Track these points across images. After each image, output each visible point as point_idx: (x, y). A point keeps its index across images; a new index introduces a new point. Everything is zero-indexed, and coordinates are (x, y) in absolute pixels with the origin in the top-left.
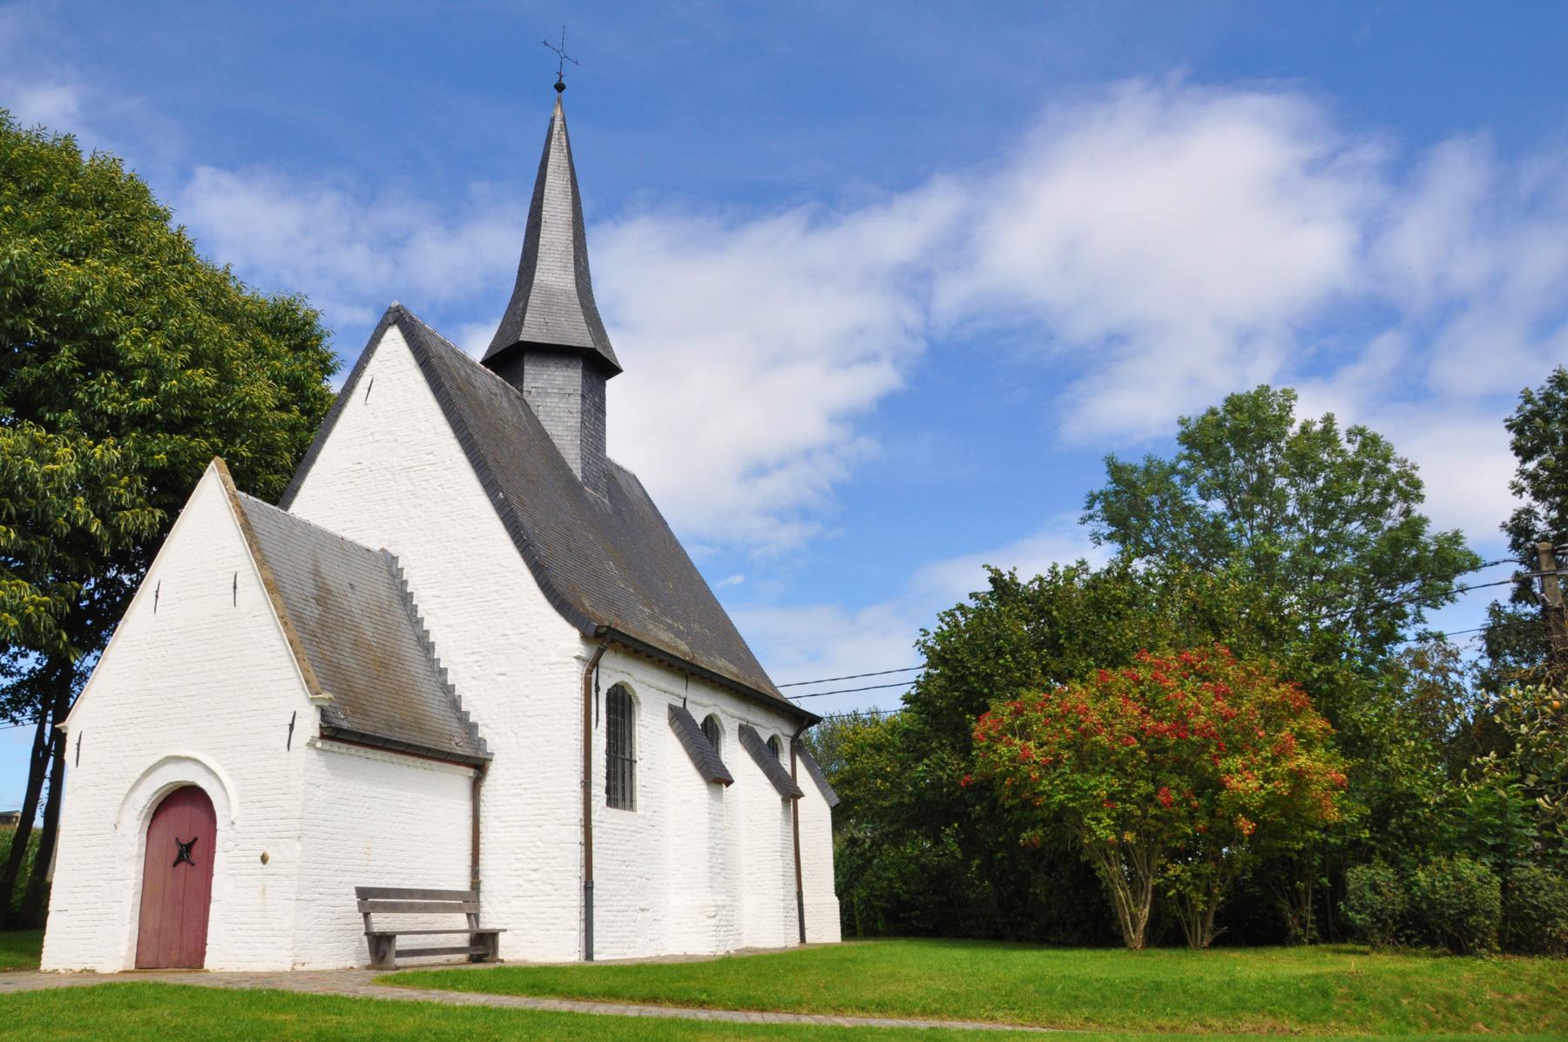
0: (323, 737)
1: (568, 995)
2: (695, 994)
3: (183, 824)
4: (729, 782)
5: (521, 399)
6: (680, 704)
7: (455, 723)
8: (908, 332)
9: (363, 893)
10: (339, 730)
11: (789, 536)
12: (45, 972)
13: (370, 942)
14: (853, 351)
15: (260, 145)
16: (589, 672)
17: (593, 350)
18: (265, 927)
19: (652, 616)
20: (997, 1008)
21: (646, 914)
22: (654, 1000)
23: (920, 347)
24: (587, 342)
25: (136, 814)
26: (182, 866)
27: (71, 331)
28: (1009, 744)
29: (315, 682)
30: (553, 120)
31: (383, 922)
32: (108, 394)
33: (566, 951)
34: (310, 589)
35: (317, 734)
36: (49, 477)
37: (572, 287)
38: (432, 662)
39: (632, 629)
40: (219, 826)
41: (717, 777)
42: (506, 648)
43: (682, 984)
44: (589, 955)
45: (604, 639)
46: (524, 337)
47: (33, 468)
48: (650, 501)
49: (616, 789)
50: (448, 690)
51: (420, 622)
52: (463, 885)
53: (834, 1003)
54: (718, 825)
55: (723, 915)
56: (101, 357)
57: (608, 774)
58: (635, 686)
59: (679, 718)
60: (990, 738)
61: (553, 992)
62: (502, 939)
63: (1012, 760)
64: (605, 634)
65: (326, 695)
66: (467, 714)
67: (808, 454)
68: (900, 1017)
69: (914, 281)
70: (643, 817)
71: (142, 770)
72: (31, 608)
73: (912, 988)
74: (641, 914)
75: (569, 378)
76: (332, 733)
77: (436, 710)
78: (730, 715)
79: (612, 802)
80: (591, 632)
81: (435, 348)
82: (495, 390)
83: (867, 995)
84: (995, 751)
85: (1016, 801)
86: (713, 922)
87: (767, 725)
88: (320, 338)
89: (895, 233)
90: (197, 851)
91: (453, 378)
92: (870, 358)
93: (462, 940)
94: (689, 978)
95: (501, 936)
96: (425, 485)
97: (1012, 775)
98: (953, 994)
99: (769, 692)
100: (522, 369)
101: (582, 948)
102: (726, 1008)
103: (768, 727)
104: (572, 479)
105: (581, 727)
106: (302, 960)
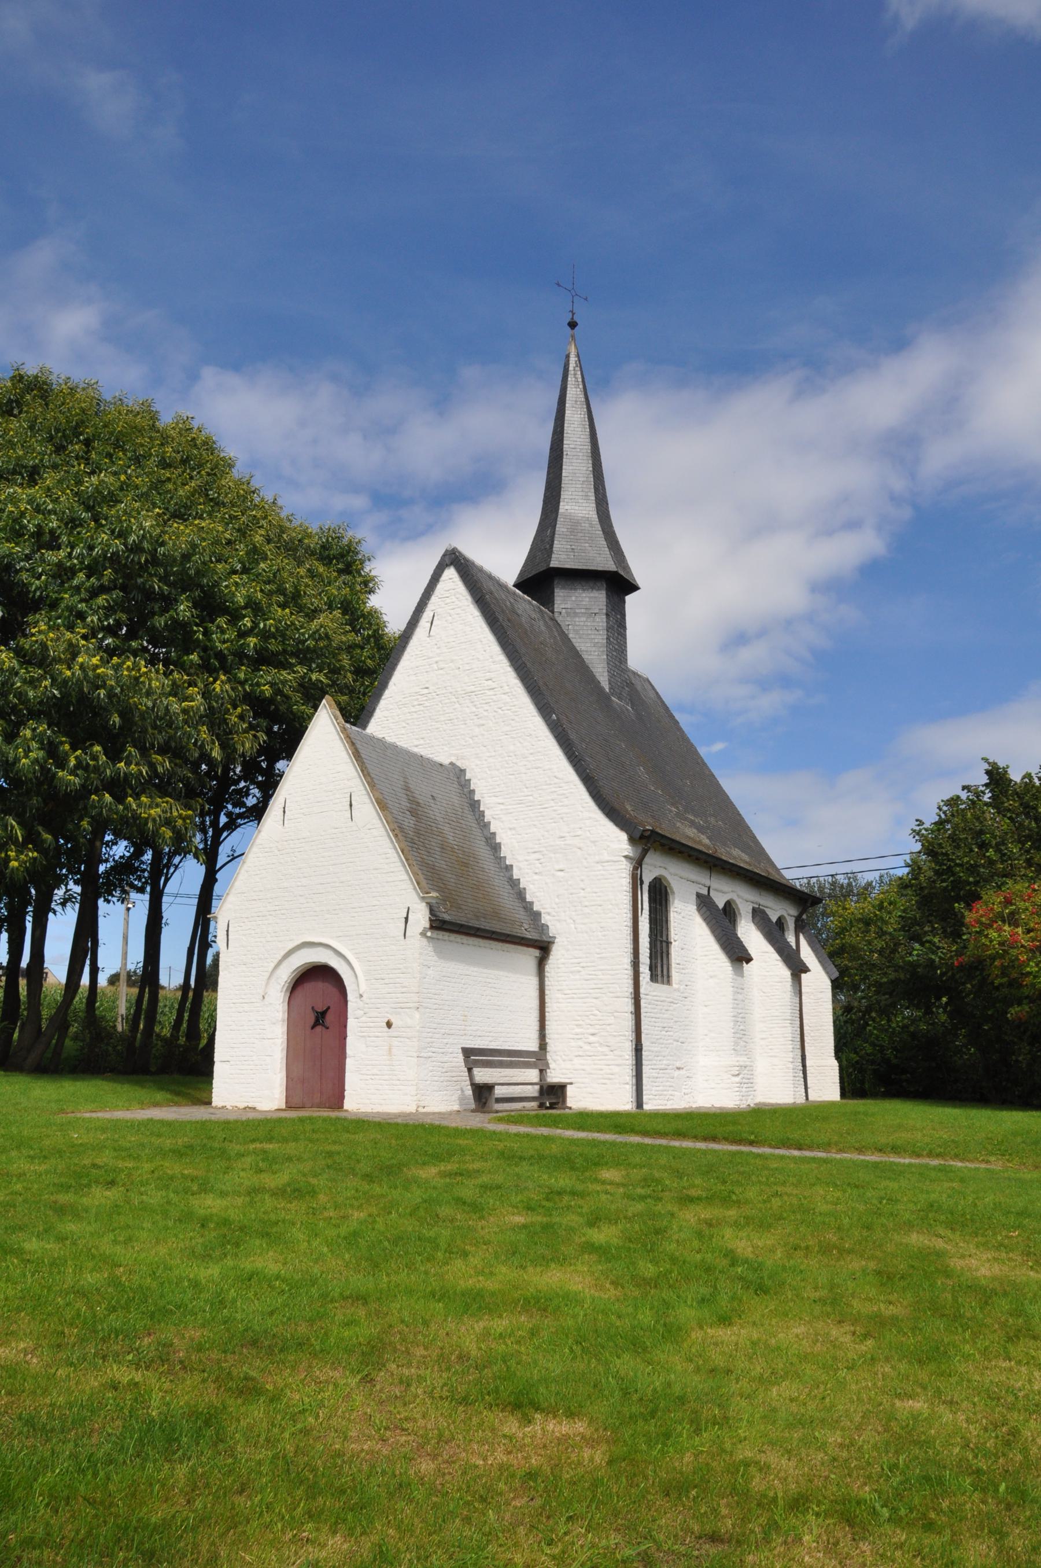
0: (432, 927)
1: (645, 1133)
2: (745, 1135)
3: (319, 996)
4: (749, 960)
5: (553, 619)
6: (705, 892)
7: (522, 912)
8: (894, 499)
9: (467, 1052)
10: (444, 922)
11: (770, 703)
12: (216, 1108)
13: (473, 1091)
14: (833, 519)
15: (264, 342)
16: (635, 869)
17: (616, 573)
18: (394, 1076)
19: (678, 815)
20: (992, 1154)
21: (681, 1072)
22: (714, 1139)
23: (906, 513)
24: (611, 566)
25: (279, 987)
26: (319, 1029)
27: (185, 583)
28: (999, 930)
29: (424, 883)
30: (568, 356)
31: (483, 1075)
32: (222, 635)
33: (622, 1101)
34: (405, 804)
35: (428, 925)
36: (185, 711)
37: (594, 515)
38: (500, 860)
39: (665, 830)
40: (350, 997)
41: (739, 956)
42: (565, 849)
43: (731, 1128)
44: (639, 1104)
45: (648, 841)
46: (554, 564)
47: (175, 707)
48: (663, 702)
49: (656, 967)
50: (514, 883)
51: (487, 825)
52: (533, 1046)
53: (857, 1145)
54: (740, 997)
55: (744, 1074)
56: (211, 605)
57: (651, 954)
58: (669, 878)
59: (704, 903)
60: (982, 923)
61: (633, 1131)
62: (570, 1090)
63: (1001, 944)
64: (648, 838)
65: (434, 894)
66: (531, 903)
67: (789, 624)
68: (911, 1157)
69: (901, 446)
70: (678, 990)
71: (283, 953)
72: (180, 822)
73: (919, 1135)
74: (677, 1072)
75: (596, 598)
76: (439, 925)
77: (507, 901)
78: (744, 898)
79: (654, 978)
80: (637, 835)
81: (487, 585)
82: (534, 616)
83: (883, 1140)
84: (986, 936)
85: (1005, 979)
86: (737, 1079)
87: (775, 907)
88: (362, 562)
89: (883, 396)
90: (330, 1018)
91: (503, 611)
92: (852, 525)
93: (533, 1091)
94: (735, 1123)
95: (569, 1088)
96: (486, 707)
97: (1002, 957)
98: (953, 1141)
99: (774, 876)
100: (553, 592)
101: (634, 1099)
102: (771, 1146)
103: (777, 909)
105: (630, 915)
106: (422, 1104)
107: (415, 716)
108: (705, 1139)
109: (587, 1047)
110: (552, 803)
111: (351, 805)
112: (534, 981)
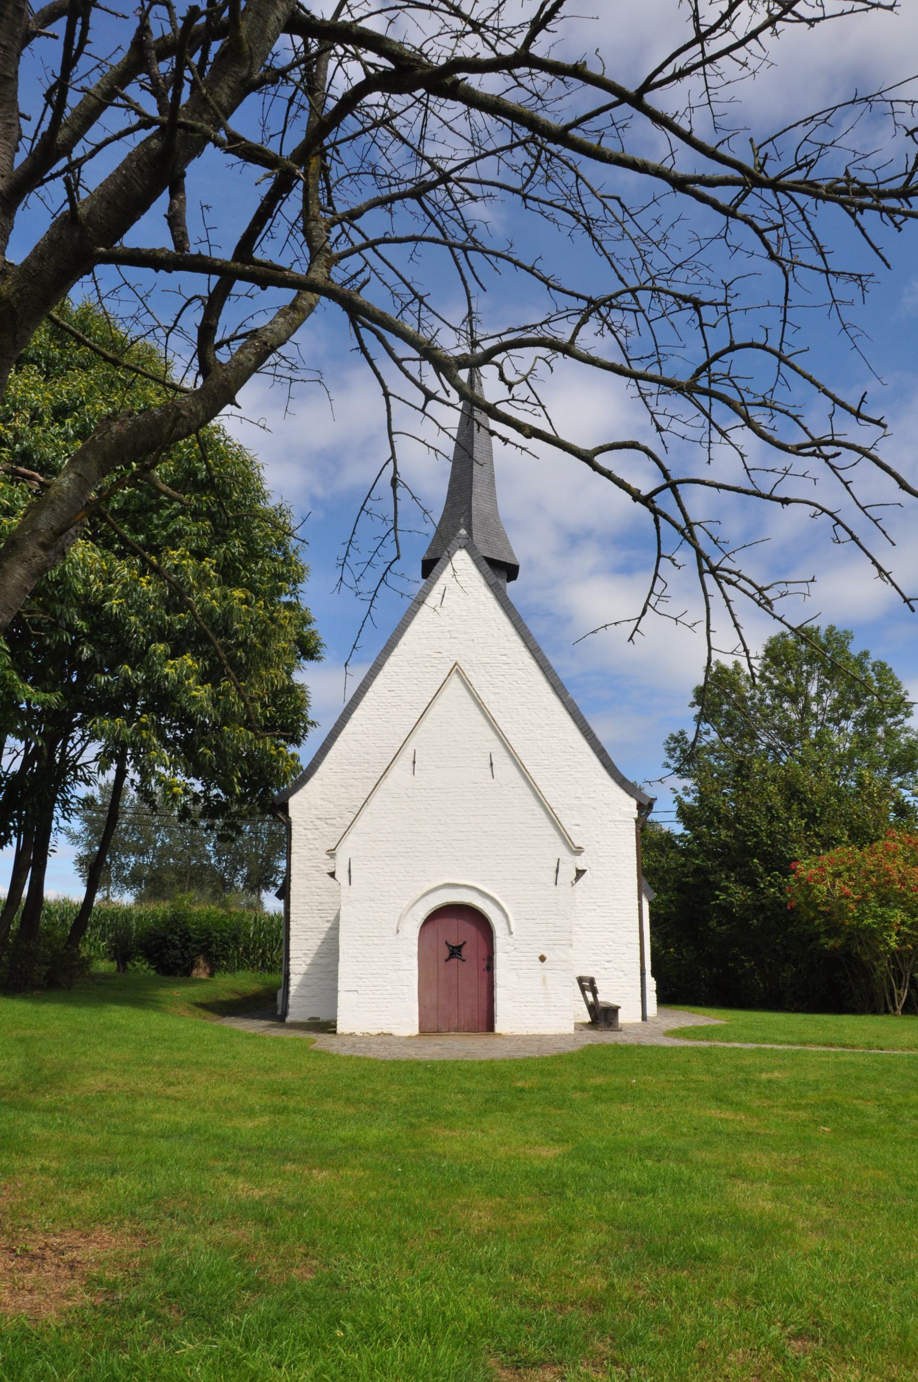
12: (342, 1034)
26: (454, 961)
96: (502, 678)
107: (428, 675)
108: (825, 1045)
109: (603, 972)
110: (568, 769)
111: (492, 764)
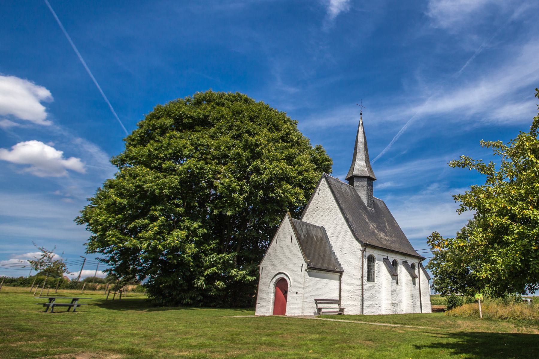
3: (282, 286)
9: (315, 300)
18: (298, 306)
31: (320, 306)
33: (357, 311)
42: (346, 247)
45: (366, 246)
52: (338, 298)
55: (394, 305)
59: (386, 260)
78: (399, 259)
79: (368, 280)
93: (338, 310)
104: (364, 206)
112: (339, 281)
